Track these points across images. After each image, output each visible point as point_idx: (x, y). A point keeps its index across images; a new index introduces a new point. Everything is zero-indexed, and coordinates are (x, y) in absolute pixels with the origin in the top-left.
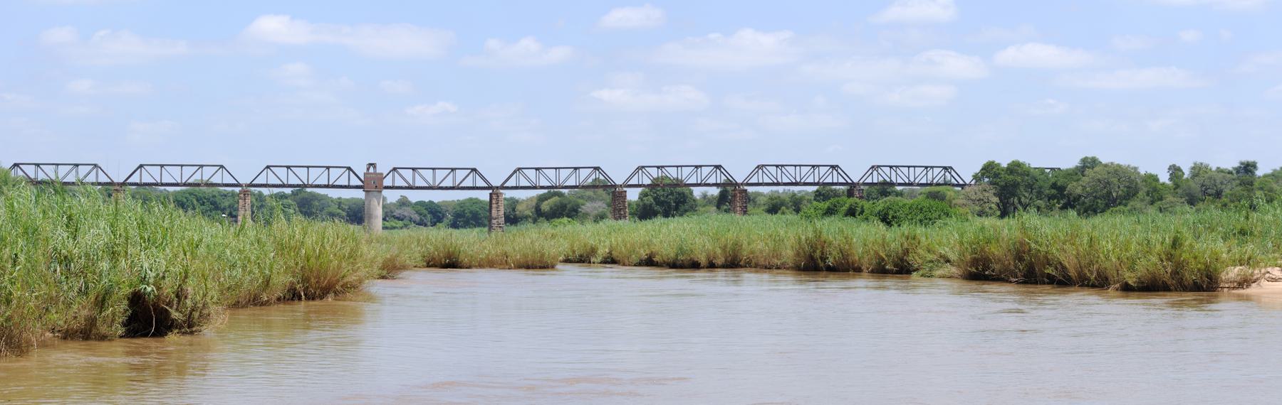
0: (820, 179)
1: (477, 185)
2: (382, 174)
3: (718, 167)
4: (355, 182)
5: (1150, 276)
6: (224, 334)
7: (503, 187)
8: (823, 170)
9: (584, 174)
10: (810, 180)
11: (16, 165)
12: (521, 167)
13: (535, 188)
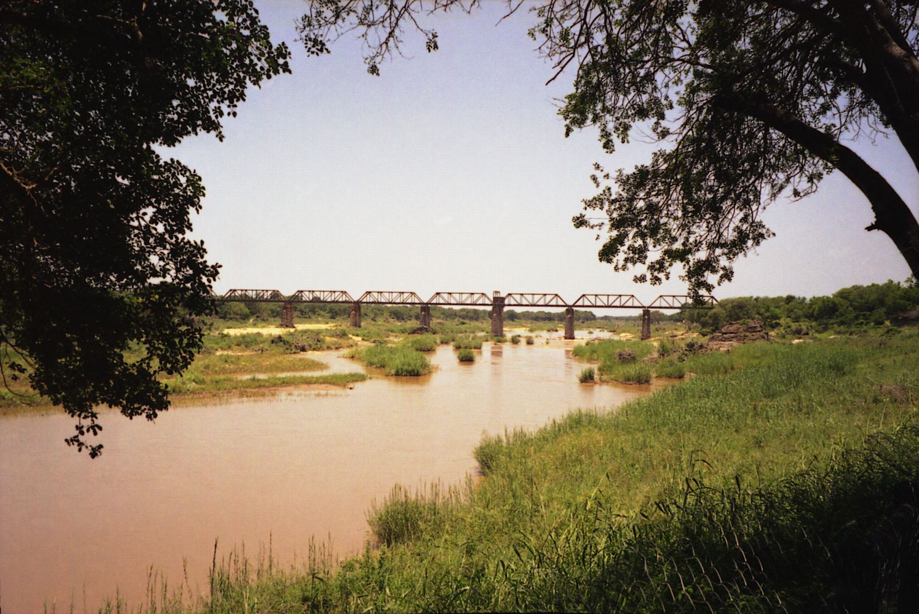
4: (487, 302)
5: (540, 575)
6: (493, 600)
7: (574, 306)
8: (394, 295)
10: (398, 301)
11: (510, 294)
13: (671, 308)
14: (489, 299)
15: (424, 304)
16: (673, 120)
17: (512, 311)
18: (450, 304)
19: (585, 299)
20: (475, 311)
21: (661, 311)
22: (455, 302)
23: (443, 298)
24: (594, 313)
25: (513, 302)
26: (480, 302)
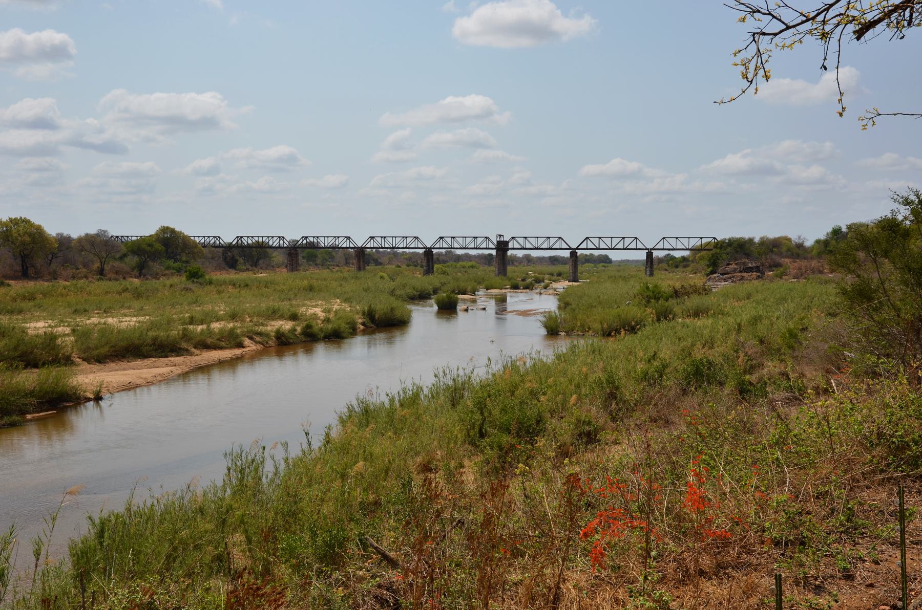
3: (416, 238)
4: (491, 246)
7: (577, 248)
9: (705, 241)
11: (513, 238)
15: (427, 248)
16: (825, 65)
18: (468, 248)
21: (672, 253)
22: (459, 247)
23: (447, 243)
25: (517, 246)
26: (484, 246)
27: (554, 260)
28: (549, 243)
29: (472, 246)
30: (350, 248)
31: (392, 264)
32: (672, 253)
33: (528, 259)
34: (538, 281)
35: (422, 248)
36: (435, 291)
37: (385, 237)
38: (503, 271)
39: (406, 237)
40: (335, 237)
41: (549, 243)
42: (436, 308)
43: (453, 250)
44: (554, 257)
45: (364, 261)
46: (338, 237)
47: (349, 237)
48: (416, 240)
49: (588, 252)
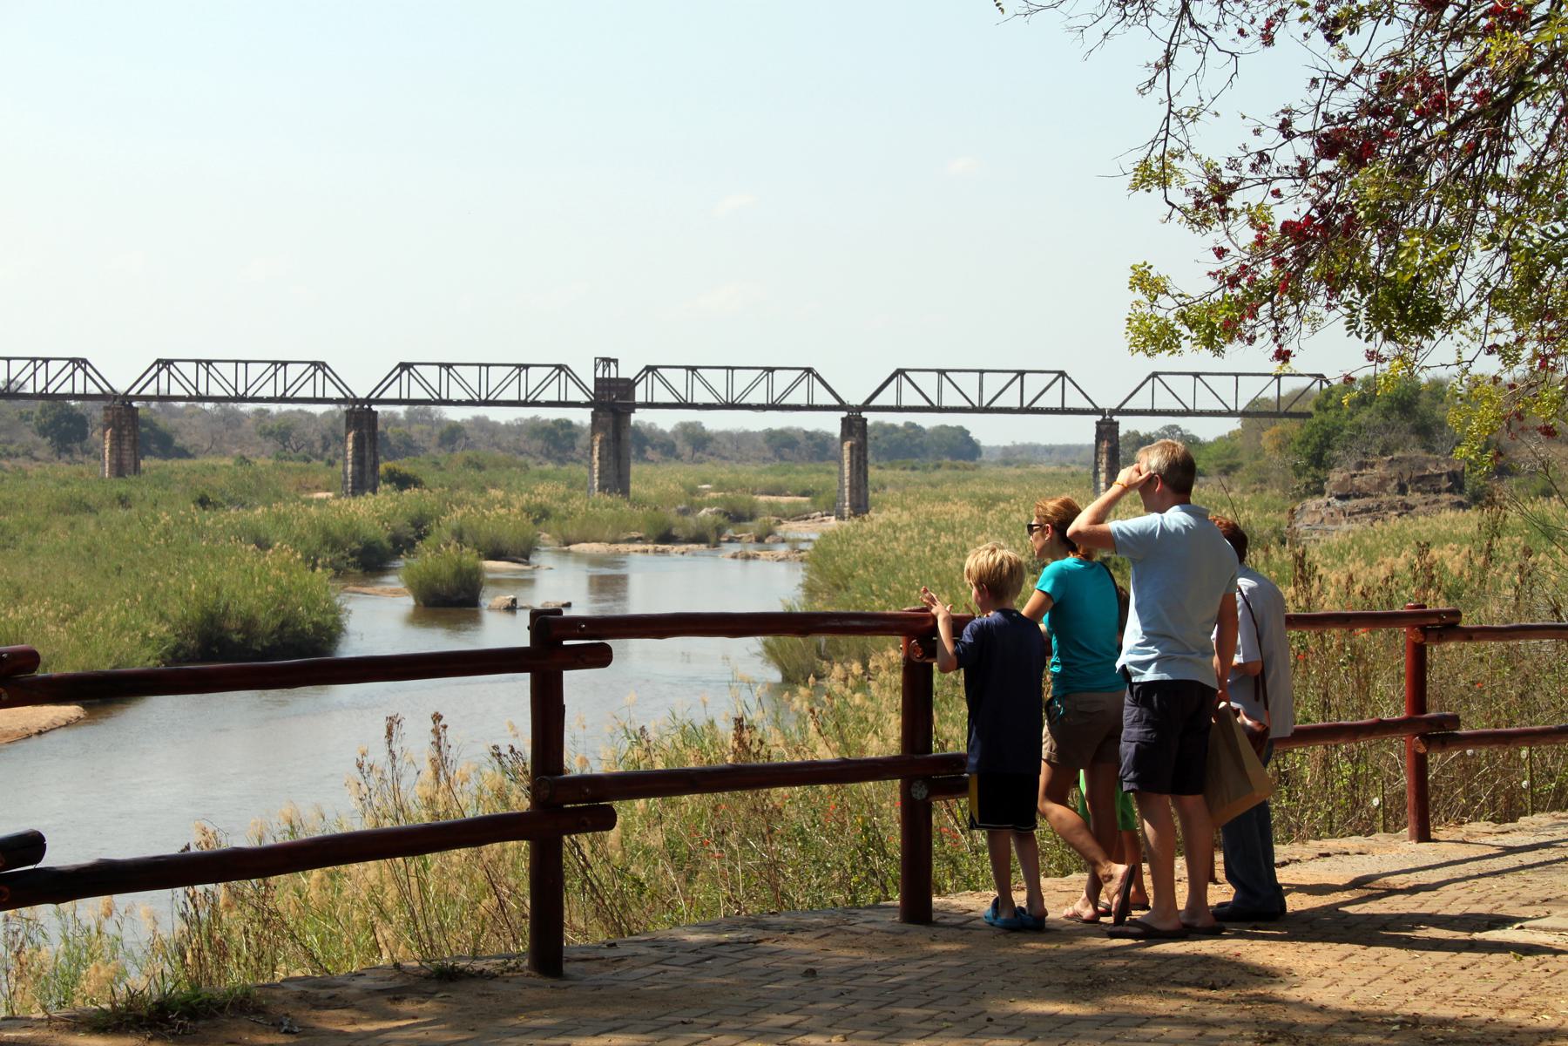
0: (286, 391)
1: (815, 403)
2: (627, 380)
3: (318, 365)
4: (576, 395)
7: (866, 407)
8: (255, 370)
11: (650, 369)
12: (985, 368)
13: (932, 409)
14: (580, 384)
15: (356, 401)
17: (696, 426)
19: (1061, 379)
20: (480, 423)
21: (1189, 425)
23: (424, 384)
24: (974, 435)
25: (662, 395)
26: (550, 394)
27: (782, 443)
28: (770, 390)
29: (511, 394)
30: (85, 397)
31: (224, 454)
32: (1189, 425)
33: (699, 441)
34: (737, 516)
35: (338, 401)
36: (402, 544)
37: (209, 362)
38: (616, 480)
39: (285, 363)
40: (34, 360)
41: (770, 390)
42: (408, 602)
43: (433, 408)
44: (782, 433)
45: (134, 443)
46: (46, 360)
47: (85, 361)
48: (563, 374)
49: (899, 419)
